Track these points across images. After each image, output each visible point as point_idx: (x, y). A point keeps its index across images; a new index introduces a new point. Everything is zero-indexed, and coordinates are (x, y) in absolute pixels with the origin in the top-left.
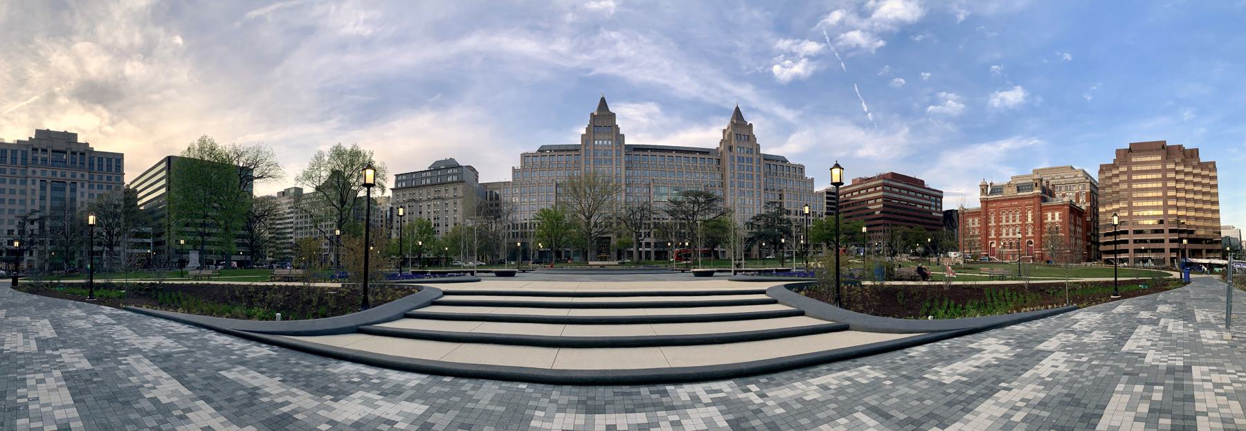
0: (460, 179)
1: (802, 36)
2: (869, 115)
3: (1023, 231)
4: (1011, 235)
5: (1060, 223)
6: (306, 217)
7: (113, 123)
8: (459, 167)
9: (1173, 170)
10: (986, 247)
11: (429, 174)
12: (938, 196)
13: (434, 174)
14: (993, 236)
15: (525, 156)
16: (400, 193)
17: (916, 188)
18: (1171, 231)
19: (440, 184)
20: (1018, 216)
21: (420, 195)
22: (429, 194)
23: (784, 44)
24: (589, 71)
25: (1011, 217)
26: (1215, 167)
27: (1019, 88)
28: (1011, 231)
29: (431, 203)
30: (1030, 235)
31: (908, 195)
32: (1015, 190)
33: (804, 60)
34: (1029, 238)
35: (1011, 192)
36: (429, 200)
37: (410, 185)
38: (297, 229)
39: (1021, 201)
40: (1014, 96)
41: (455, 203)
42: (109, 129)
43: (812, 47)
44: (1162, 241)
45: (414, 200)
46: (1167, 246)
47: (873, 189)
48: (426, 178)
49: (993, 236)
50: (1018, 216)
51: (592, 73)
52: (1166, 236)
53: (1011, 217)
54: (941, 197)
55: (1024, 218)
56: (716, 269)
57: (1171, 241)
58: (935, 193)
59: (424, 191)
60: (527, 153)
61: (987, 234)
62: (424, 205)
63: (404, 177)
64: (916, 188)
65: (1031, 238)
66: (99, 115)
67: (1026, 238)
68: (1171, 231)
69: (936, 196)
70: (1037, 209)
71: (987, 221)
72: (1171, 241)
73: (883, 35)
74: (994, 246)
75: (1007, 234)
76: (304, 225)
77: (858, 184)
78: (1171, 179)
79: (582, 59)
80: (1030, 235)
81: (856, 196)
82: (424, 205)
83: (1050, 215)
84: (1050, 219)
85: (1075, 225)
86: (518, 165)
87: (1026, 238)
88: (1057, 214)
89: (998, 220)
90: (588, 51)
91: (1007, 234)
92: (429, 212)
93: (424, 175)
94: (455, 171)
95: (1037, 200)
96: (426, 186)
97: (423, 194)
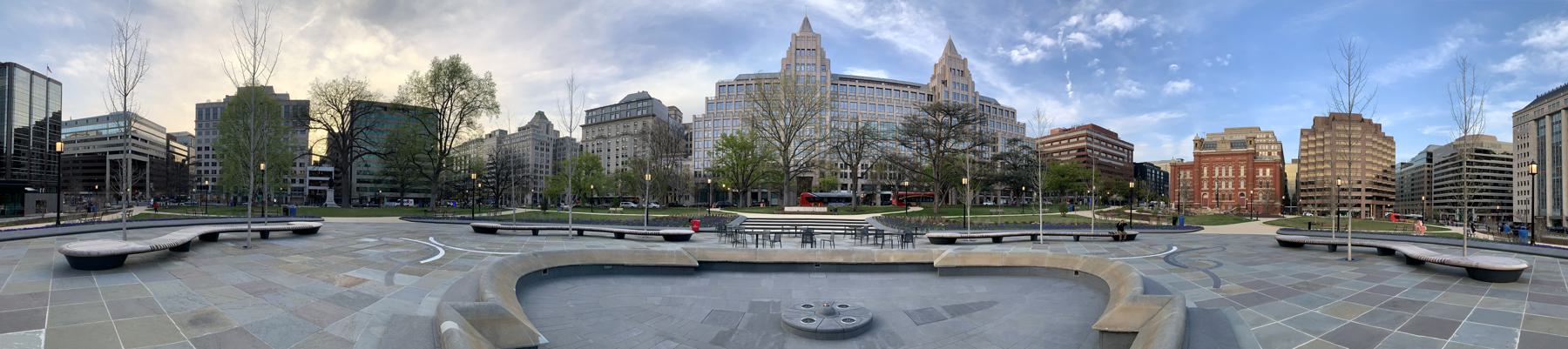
0: (650, 112)
1: (1045, 31)
2: (1071, 93)
3: (1236, 185)
4: (1223, 187)
5: (1271, 179)
6: (542, 149)
7: (397, 51)
8: (651, 99)
9: (1371, 140)
10: (1199, 197)
11: (618, 108)
12: (1129, 149)
13: (624, 107)
14: (1205, 188)
15: (720, 86)
16: (590, 130)
17: (1108, 139)
18: (1367, 190)
19: (605, 123)
20: (1230, 170)
21: (609, 130)
22: (618, 130)
23: (1028, 36)
24: (869, 33)
25: (1224, 170)
26: (1302, 134)
27: (1188, 81)
28: (1223, 183)
29: (595, 143)
30: (1242, 187)
31: (1106, 146)
32: (1229, 146)
33: (1039, 51)
34: (1241, 190)
35: (1226, 148)
36: (618, 136)
37: (624, 116)
38: (849, 141)
39: (1234, 157)
40: (1182, 86)
41: (617, 142)
42: (391, 58)
43: (1047, 41)
44: (1360, 198)
45: (602, 137)
46: (1364, 202)
47: (1057, 143)
48: (616, 113)
49: (1205, 188)
50: (1230, 170)
51: (873, 36)
52: (1363, 194)
53: (1224, 170)
54: (1132, 151)
55: (1237, 172)
56: (959, 235)
57: (1367, 198)
58: (1122, 144)
59: (613, 127)
60: (723, 82)
61: (1200, 186)
62: (613, 142)
63: (594, 113)
64: (1108, 139)
65: (1243, 190)
66: (382, 41)
67: (1239, 190)
68: (1367, 190)
69: (1128, 149)
70: (1250, 165)
71: (1201, 172)
72: (1367, 198)
73: (1101, 39)
74: (1205, 197)
75: (1227, 186)
76: (544, 158)
77: (1056, 135)
78: (1369, 147)
79: (868, 22)
80: (1242, 187)
81: (1057, 146)
82: (613, 142)
83: (1261, 170)
84: (1261, 175)
85: (1025, 147)
86: (712, 94)
87: (1239, 190)
88: (1268, 170)
89: (1211, 172)
90: (873, 16)
91: (1227, 186)
92: (617, 150)
93: (613, 109)
94: (645, 104)
95: (1251, 157)
96: (615, 121)
97: (612, 130)
